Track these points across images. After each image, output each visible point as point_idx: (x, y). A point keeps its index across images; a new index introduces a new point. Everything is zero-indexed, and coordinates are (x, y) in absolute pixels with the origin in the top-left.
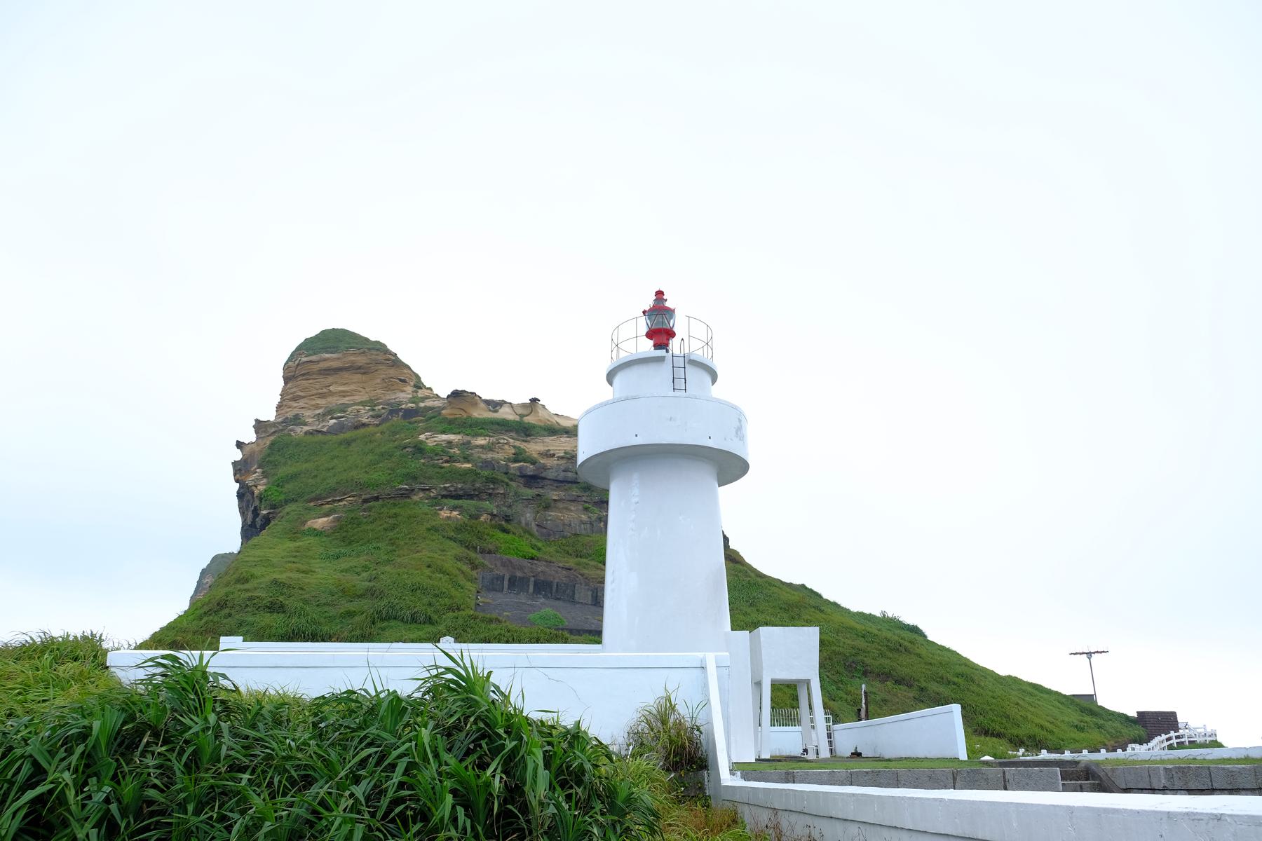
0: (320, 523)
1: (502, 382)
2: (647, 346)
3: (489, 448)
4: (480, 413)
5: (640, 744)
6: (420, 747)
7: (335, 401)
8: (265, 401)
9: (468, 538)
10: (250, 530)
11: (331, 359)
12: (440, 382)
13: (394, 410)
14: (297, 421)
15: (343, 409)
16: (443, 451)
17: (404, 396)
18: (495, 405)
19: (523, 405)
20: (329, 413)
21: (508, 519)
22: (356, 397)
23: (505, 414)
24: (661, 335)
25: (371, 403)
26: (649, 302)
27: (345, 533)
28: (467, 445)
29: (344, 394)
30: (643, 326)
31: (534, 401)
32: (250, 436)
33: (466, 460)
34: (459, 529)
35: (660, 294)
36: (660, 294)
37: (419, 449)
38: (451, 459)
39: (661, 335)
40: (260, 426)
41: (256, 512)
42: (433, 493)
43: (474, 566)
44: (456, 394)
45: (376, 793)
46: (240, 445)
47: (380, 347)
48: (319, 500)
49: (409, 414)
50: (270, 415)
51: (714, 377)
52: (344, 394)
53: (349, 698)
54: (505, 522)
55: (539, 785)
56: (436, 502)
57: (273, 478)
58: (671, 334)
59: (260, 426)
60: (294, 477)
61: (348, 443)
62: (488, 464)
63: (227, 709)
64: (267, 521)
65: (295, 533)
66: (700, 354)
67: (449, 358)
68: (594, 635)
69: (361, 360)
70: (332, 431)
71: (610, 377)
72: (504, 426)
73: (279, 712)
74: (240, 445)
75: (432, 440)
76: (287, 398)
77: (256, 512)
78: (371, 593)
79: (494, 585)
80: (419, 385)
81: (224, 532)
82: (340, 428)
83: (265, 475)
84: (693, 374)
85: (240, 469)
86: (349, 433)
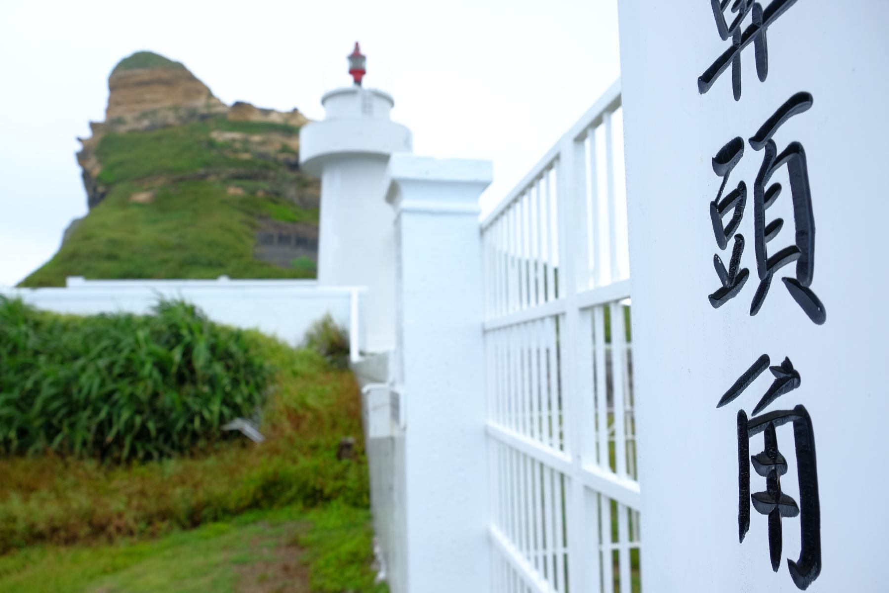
0: (142, 197)
1: (270, 96)
2: (348, 81)
3: (263, 143)
4: (256, 118)
5: (311, 340)
6: (137, 341)
7: (148, 107)
8: (95, 106)
9: (248, 207)
10: (93, 201)
11: (142, 74)
12: (227, 94)
13: (193, 114)
14: (120, 121)
15: (154, 112)
16: (229, 145)
17: (200, 103)
18: (266, 112)
19: (288, 113)
20: (144, 115)
21: (278, 194)
22: (164, 104)
23: (274, 118)
24: (358, 73)
25: (176, 108)
26: (350, 50)
27: (161, 205)
28: (245, 142)
29: (154, 101)
30: (346, 65)
31: (295, 111)
32: (87, 133)
33: (246, 151)
34: (243, 201)
35: (357, 44)
36: (357, 44)
37: (211, 144)
38: (236, 151)
39: (358, 73)
40: (93, 126)
41: (95, 189)
42: (223, 176)
43: (253, 227)
44: (239, 105)
45: (110, 367)
46: (80, 140)
47: (179, 67)
48: (140, 180)
49: (204, 117)
50: (100, 117)
51: (391, 102)
52: (154, 101)
53: (102, 316)
54: (275, 196)
55: (201, 356)
56: (227, 181)
57: (106, 161)
58: (363, 72)
59: (93, 126)
60: (121, 164)
61: (159, 139)
62: (263, 156)
63: (37, 325)
64: (103, 196)
65: (124, 203)
66: (383, 88)
67: (231, 79)
68: (310, 273)
69: (166, 75)
70: (148, 129)
71: (324, 101)
72: (273, 127)
73: (69, 325)
74: (80, 140)
75: (222, 136)
76: (113, 103)
77: (95, 189)
78: (180, 247)
79: (267, 240)
80: (210, 95)
81: (75, 203)
82: (152, 128)
83: (100, 161)
84: (377, 103)
85: (82, 157)
86: (159, 132)
